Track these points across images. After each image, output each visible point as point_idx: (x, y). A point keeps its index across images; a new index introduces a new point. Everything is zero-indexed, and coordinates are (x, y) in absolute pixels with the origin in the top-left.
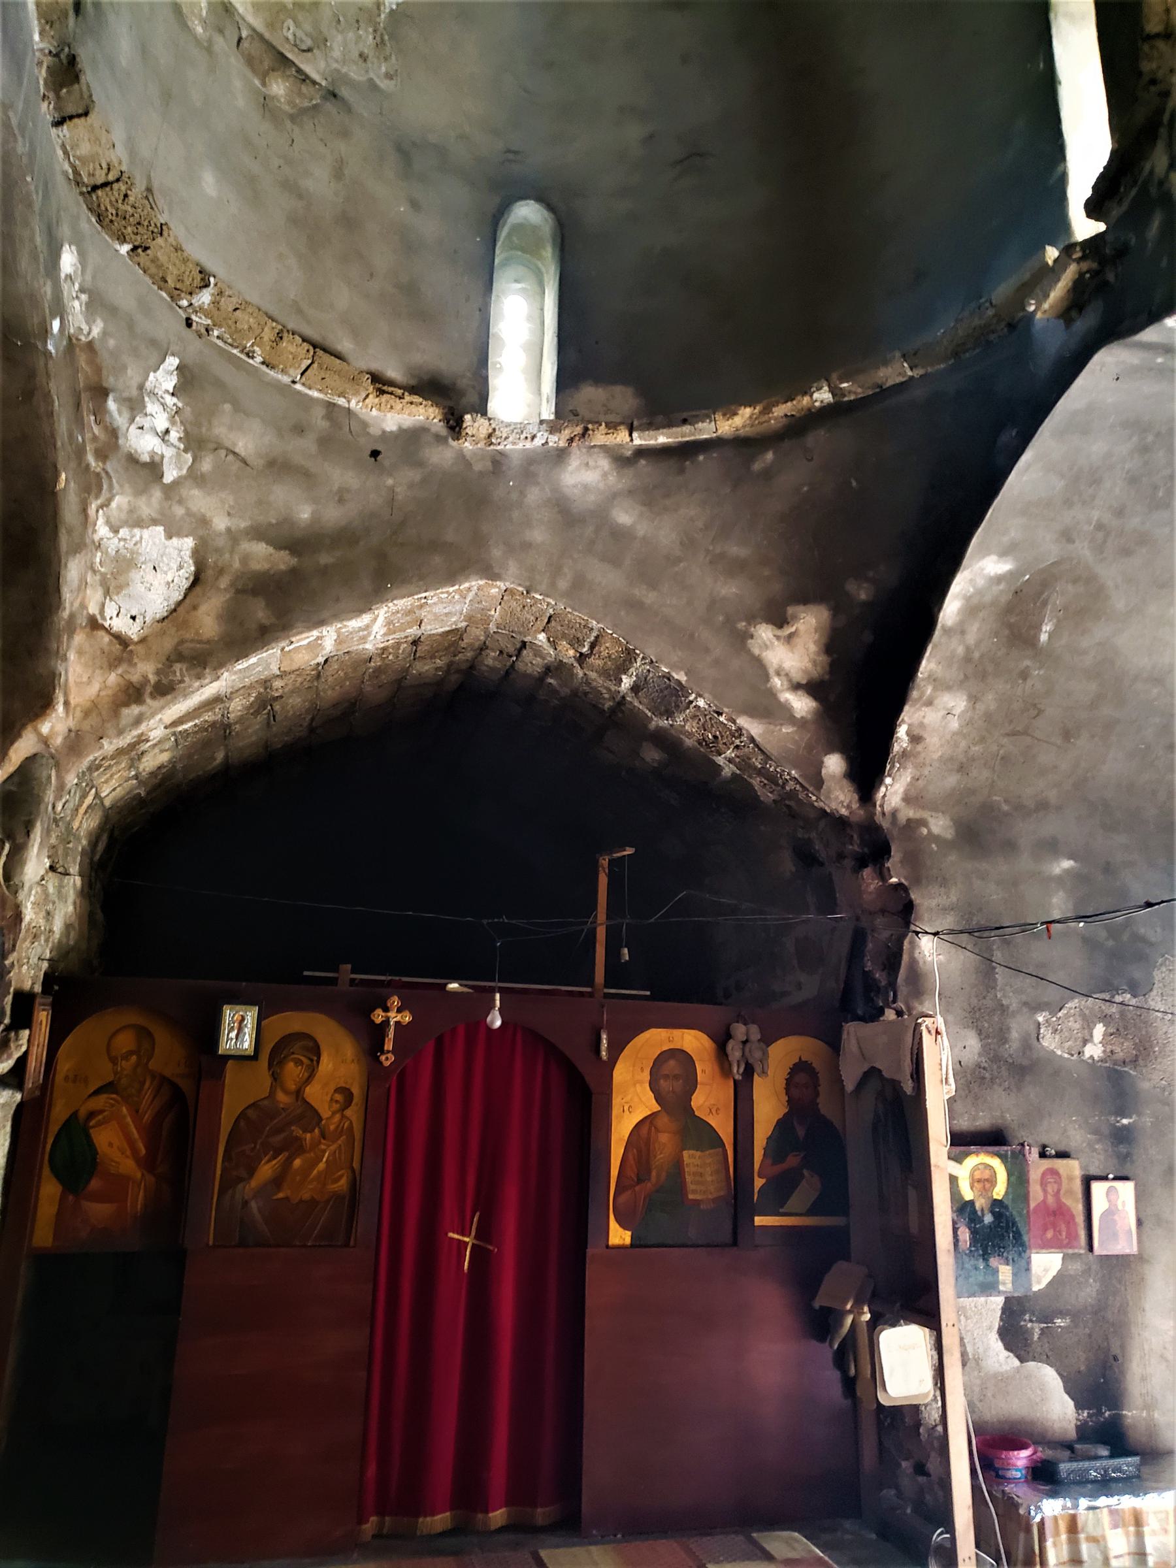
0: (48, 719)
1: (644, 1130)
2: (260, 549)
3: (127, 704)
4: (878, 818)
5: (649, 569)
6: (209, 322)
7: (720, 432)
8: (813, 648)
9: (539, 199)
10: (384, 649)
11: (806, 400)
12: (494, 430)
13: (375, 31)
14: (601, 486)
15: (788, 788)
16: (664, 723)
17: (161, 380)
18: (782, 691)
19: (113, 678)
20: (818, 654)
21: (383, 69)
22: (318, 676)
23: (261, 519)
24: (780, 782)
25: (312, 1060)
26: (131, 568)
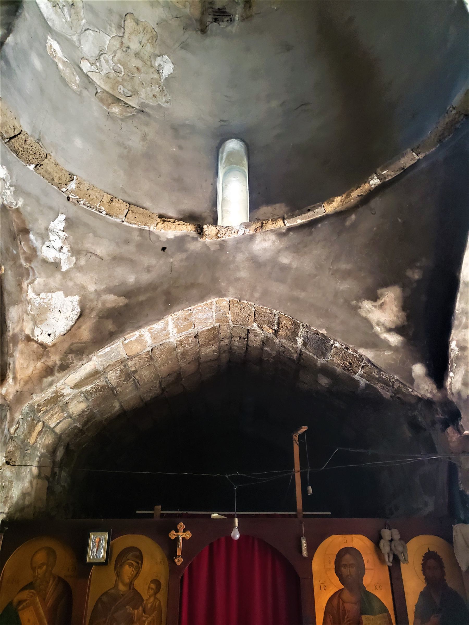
0: (5, 386)
1: (335, 602)
2: (111, 297)
3: (46, 377)
4: (450, 397)
5: (300, 282)
6: (77, 197)
7: (327, 212)
8: (395, 309)
9: (237, 137)
10: (181, 341)
11: (367, 186)
12: (219, 231)
13: (159, 86)
14: (272, 247)
15: (395, 387)
16: (323, 361)
17: (57, 225)
18: (382, 333)
19: (39, 365)
20: (399, 312)
21: (164, 100)
22: (151, 358)
23: (111, 284)
24: (391, 383)
25: (138, 563)
26: (50, 312)
